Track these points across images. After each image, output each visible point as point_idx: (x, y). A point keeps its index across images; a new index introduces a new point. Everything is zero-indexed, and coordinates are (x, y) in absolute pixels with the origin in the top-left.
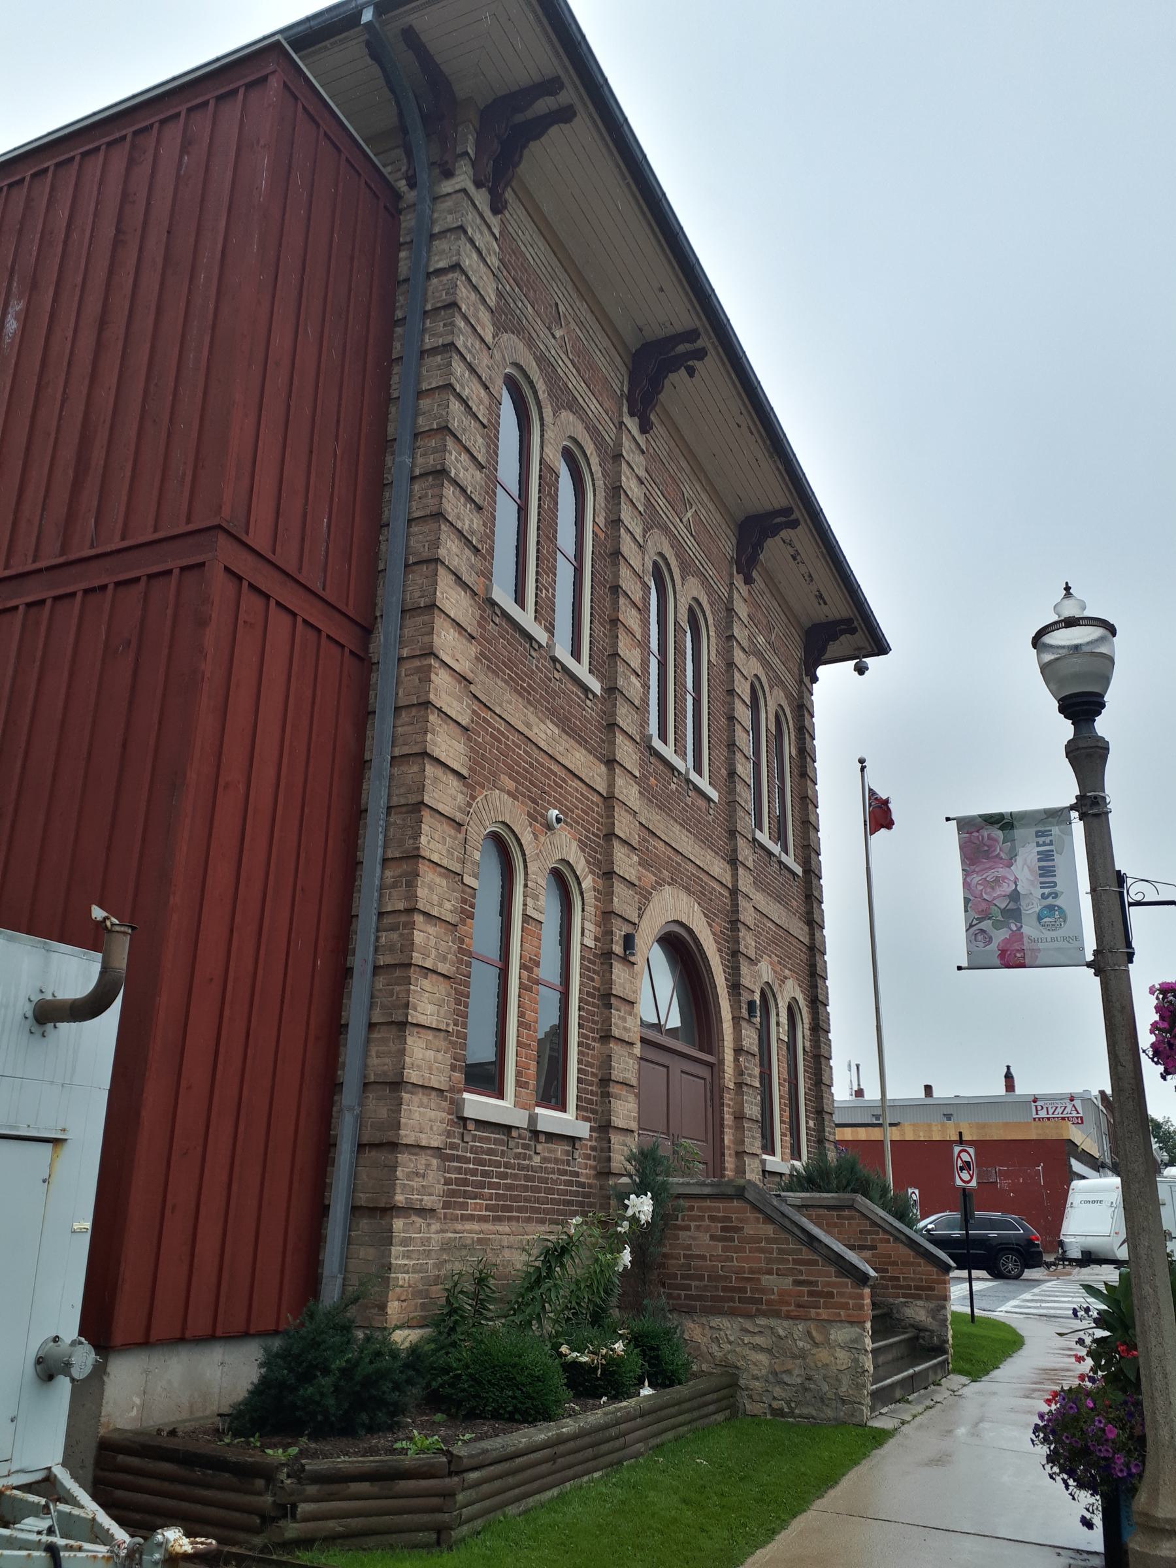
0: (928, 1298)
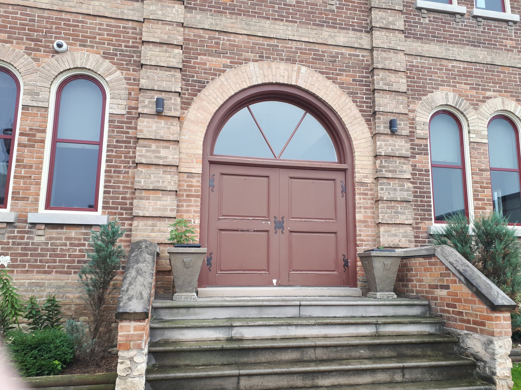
0: (482, 332)
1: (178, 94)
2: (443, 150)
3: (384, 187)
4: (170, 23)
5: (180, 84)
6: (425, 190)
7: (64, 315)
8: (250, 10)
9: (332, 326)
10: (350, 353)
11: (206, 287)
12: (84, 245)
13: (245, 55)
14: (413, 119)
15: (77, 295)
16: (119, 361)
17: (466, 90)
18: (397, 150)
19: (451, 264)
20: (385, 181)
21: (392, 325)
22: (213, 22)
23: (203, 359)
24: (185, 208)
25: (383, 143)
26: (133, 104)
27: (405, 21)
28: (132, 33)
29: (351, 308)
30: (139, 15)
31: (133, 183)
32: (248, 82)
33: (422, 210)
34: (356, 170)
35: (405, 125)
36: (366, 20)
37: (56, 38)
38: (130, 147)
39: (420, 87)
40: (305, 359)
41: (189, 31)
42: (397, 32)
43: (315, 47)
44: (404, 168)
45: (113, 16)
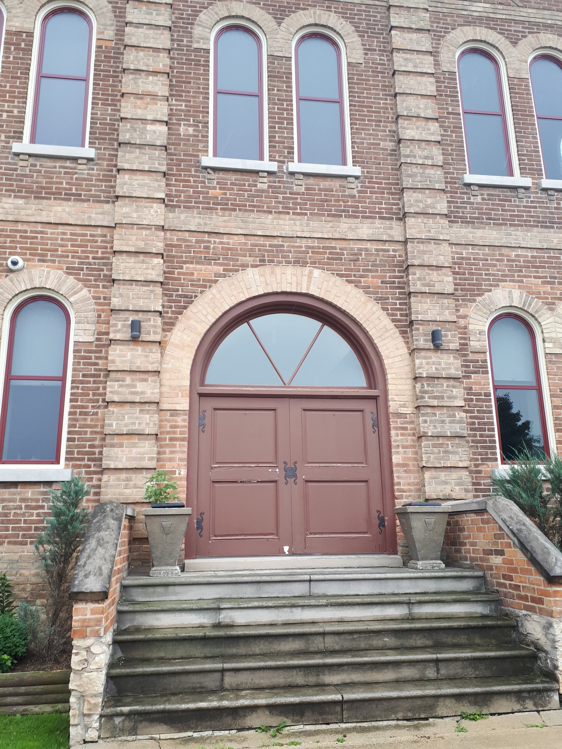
0: (542, 612)
3: (428, 419)
4: (148, 227)
5: (161, 301)
6: (486, 420)
7: (17, 597)
9: (349, 607)
10: (370, 642)
12: (42, 507)
13: (242, 260)
14: (465, 327)
15: (33, 572)
16: (74, 651)
17: (536, 285)
18: (444, 369)
19: (504, 521)
20: (429, 410)
21: (431, 604)
22: (201, 221)
23: (181, 651)
24: (167, 456)
25: (424, 361)
26: (103, 328)
27: (448, 202)
28: (102, 241)
29: (377, 583)
31: (103, 427)
32: (246, 292)
33: (482, 447)
34: (390, 397)
35: (453, 336)
36: (398, 204)
37: (11, 254)
38: (100, 382)
39: (473, 285)
40: (312, 649)
41: (171, 235)
42: (438, 216)
43: (331, 243)
44: (454, 393)
45: (79, 223)
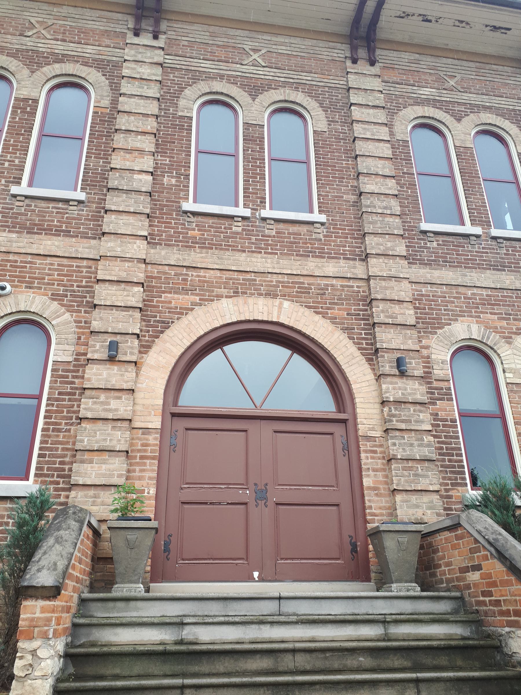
1: (136, 336)
2: (471, 393)
3: (397, 442)
4: (131, 260)
5: (139, 324)
6: (453, 445)
8: (223, 243)
9: (321, 625)
11: (162, 582)
13: (217, 291)
14: (428, 357)
18: (410, 394)
19: (479, 532)
20: (397, 433)
21: (408, 624)
23: (138, 667)
24: (137, 474)
26: (82, 349)
27: (407, 246)
30: (95, 253)
31: (74, 444)
32: (220, 319)
33: (451, 472)
34: (359, 420)
35: (417, 364)
36: (360, 247)
39: (434, 319)
40: (281, 669)
44: (421, 417)
45: (66, 255)
